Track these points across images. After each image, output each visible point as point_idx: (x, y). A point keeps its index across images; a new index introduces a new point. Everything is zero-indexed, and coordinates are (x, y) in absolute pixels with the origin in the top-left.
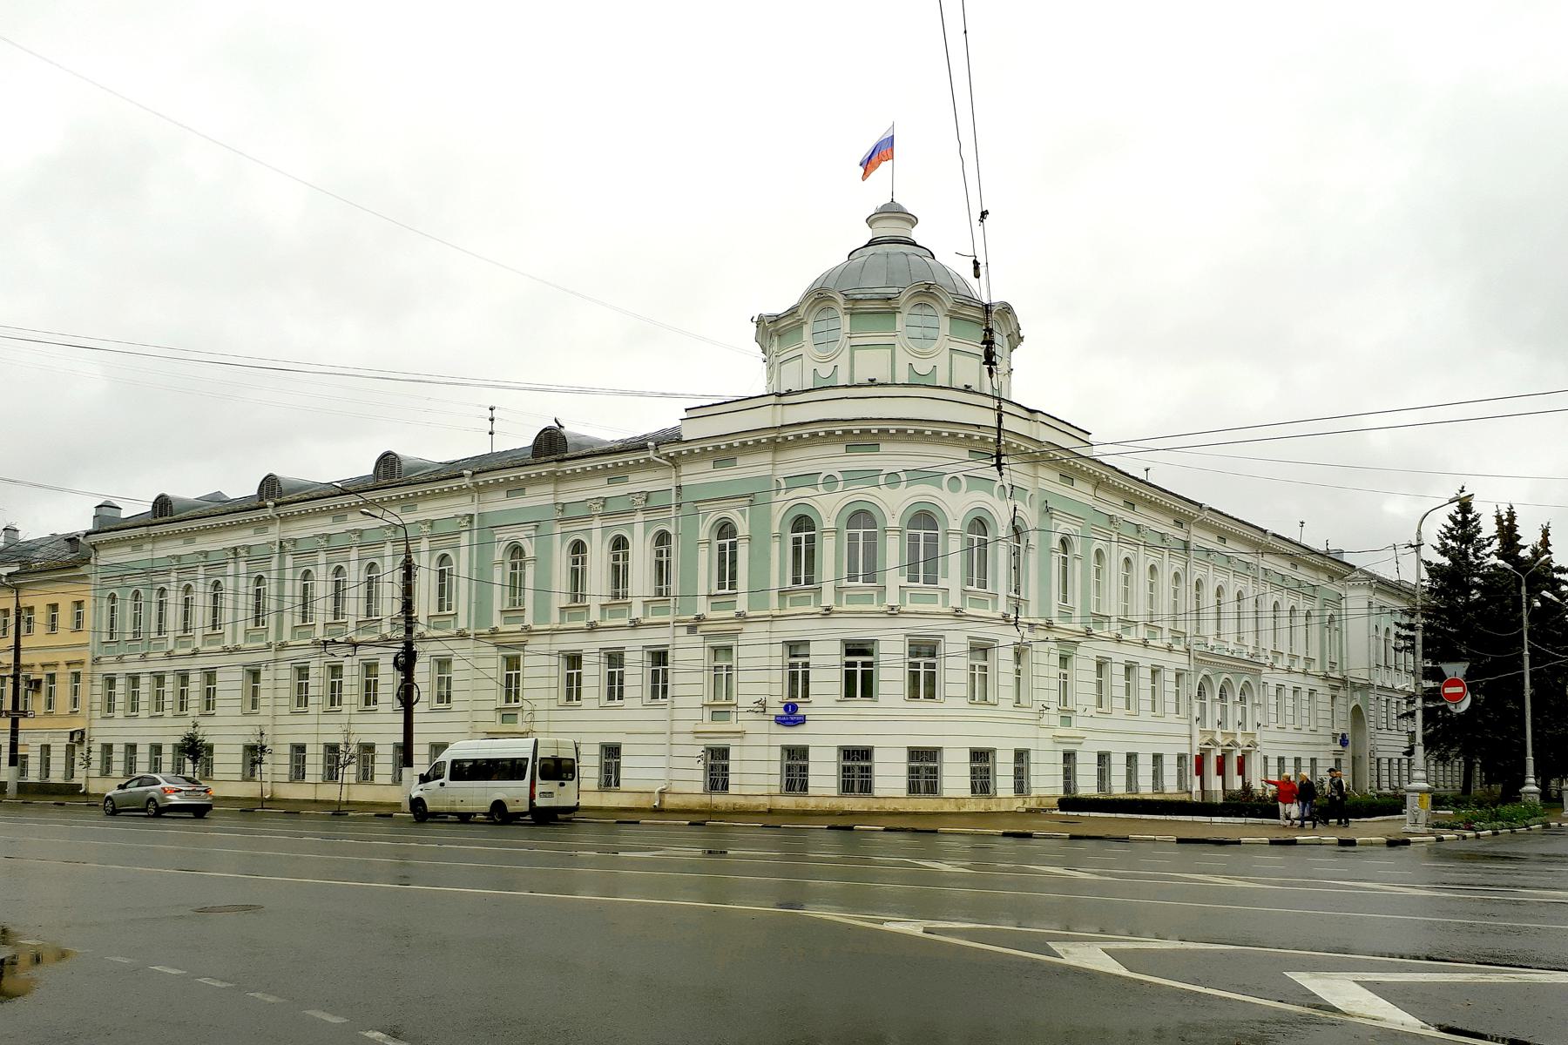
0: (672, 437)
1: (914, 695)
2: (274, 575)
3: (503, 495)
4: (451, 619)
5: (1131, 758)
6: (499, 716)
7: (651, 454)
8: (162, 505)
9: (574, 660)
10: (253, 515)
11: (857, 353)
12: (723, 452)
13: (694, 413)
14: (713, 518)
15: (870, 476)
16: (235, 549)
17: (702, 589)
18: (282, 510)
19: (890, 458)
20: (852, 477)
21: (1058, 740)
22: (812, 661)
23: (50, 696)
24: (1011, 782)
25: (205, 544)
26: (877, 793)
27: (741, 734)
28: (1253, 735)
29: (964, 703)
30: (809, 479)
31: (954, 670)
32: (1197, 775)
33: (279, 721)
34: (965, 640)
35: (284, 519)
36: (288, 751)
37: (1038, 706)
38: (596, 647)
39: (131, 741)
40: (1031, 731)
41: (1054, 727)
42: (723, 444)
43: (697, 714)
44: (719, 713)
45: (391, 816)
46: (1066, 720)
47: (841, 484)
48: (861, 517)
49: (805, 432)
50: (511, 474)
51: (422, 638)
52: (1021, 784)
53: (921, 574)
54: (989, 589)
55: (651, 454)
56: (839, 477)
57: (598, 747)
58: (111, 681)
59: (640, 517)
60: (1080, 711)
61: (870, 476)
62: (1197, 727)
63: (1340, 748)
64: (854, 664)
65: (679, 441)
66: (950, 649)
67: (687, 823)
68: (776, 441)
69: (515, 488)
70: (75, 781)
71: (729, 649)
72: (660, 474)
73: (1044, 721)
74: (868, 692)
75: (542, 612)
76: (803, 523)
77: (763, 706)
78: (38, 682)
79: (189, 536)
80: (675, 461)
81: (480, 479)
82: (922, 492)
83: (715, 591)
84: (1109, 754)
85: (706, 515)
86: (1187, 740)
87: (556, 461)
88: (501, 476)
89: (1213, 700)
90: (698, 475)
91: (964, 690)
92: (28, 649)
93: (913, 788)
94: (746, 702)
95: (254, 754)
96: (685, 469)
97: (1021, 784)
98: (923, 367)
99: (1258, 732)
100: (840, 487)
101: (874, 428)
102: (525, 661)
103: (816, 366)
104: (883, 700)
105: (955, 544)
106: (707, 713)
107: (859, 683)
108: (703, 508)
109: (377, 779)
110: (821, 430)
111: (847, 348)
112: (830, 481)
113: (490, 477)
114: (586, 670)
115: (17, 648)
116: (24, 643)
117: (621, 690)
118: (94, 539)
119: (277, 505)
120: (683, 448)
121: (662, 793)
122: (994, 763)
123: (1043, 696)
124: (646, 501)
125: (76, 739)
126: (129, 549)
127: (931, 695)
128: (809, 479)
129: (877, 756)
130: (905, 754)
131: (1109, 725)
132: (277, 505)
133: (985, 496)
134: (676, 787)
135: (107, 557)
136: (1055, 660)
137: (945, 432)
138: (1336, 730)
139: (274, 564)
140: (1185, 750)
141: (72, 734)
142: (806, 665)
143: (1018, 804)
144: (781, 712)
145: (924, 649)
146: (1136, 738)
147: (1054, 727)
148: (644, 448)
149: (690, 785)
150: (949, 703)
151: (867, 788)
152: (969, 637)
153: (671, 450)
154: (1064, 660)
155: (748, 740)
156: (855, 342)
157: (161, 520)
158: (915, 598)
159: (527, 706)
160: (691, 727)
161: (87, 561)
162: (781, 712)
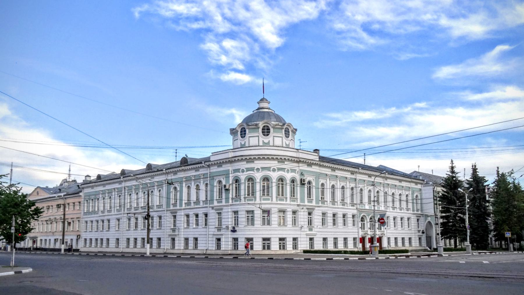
0: (207, 160)
1: (264, 224)
2: (123, 194)
3: (172, 174)
4: (161, 206)
5: (396, 239)
6: (172, 231)
7: (203, 164)
8: (99, 177)
9: (188, 216)
10: (118, 180)
11: (275, 138)
12: (220, 164)
13: (214, 154)
14: (217, 180)
15: (252, 169)
16: (114, 188)
17: (215, 198)
18: (125, 179)
19: (258, 164)
20: (248, 170)
21: (307, 235)
22: (239, 216)
23: (206, 223)
24: (401, 244)
25: (108, 187)
26: (272, 249)
27: (315, 235)
28: (384, 231)
29: (277, 226)
30: (268, 169)
31: (275, 217)
32: (369, 243)
33: (124, 232)
34: (277, 210)
35: (125, 181)
36: (244, 241)
37: (300, 226)
38: (201, 212)
39: (325, 237)
40: (299, 233)
41: (306, 231)
42: (283, 158)
43: (214, 230)
44: (219, 229)
45: (180, 257)
46: (311, 230)
47: (277, 171)
48: (266, 179)
49: (236, 159)
50: (174, 170)
51: (62, 215)
52: (295, 247)
53: (266, 194)
54: (295, 197)
55: (203, 164)
56: (276, 169)
57: (244, 239)
58: (86, 222)
59: (202, 180)
60: (315, 227)
61: (252, 169)
62: (360, 230)
63: (421, 234)
64: (265, 216)
65: (210, 161)
66: (273, 212)
67: (384, 258)
68: (231, 161)
69: (175, 173)
70: (78, 248)
71: (220, 213)
72: (205, 169)
73: (303, 230)
74: (269, 224)
75: (181, 205)
76: (237, 181)
77: (227, 228)
78: (70, 223)
79: (104, 185)
80: (209, 166)
81: (167, 171)
82: (281, 173)
83: (218, 199)
84: (327, 238)
85: (216, 179)
86: (357, 233)
87: (184, 166)
88: (172, 170)
89: (367, 222)
90: (214, 169)
91: (291, 223)
92: (68, 214)
93: (264, 248)
94: (224, 227)
95: (266, 240)
96: (211, 168)
97: (295, 247)
98: (266, 141)
99: (385, 231)
100: (260, 171)
101: (252, 157)
102: (223, 214)
103: (241, 142)
104: (255, 226)
105: (274, 184)
106: (216, 230)
107: (251, 220)
108: (215, 178)
109: (130, 247)
110: (240, 158)
111: (272, 137)
112: (258, 169)
113: (169, 170)
114: (191, 219)
115: (64, 215)
116: (66, 213)
117: (238, 223)
118: (83, 186)
119: (123, 177)
120: (210, 163)
121: (206, 250)
122: (286, 241)
123: (302, 223)
124: (203, 176)
125: (78, 237)
126: (90, 189)
127: (269, 224)
128: (268, 169)
129: (254, 240)
130: (278, 240)
131: (338, 230)
132: (123, 177)
133: (283, 173)
134: (210, 248)
135: (86, 191)
136: (307, 213)
137: (261, 157)
138: (420, 229)
139: (123, 192)
140: (357, 236)
141: (78, 236)
142: (238, 217)
143: (294, 252)
144: (232, 229)
145: (267, 212)
146: (336, 233)
147: (306, 231)
148: (202, 163)
149: (212, 247)
150: (273, 226)
151: (269, 248)
152: (278, 209)
153: (207, 163)
154: (310, 214)
155: (317, 236)
156: (274, 135)
157: (98, 181)
158: (264, 200)
159: (177, 228)
160: (212, 233)
161: (81, 192)
162: (232, 229)
